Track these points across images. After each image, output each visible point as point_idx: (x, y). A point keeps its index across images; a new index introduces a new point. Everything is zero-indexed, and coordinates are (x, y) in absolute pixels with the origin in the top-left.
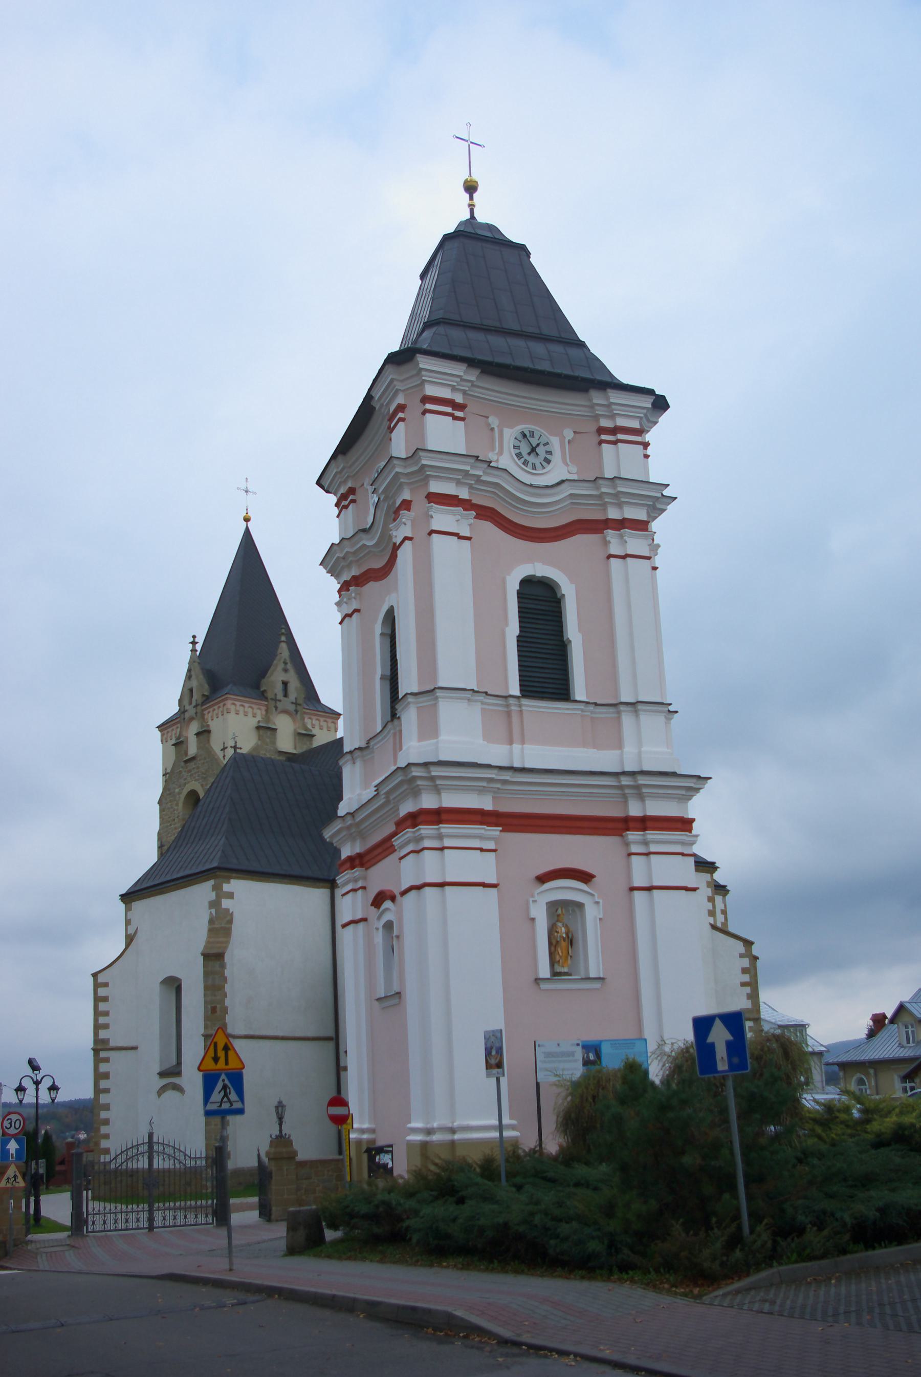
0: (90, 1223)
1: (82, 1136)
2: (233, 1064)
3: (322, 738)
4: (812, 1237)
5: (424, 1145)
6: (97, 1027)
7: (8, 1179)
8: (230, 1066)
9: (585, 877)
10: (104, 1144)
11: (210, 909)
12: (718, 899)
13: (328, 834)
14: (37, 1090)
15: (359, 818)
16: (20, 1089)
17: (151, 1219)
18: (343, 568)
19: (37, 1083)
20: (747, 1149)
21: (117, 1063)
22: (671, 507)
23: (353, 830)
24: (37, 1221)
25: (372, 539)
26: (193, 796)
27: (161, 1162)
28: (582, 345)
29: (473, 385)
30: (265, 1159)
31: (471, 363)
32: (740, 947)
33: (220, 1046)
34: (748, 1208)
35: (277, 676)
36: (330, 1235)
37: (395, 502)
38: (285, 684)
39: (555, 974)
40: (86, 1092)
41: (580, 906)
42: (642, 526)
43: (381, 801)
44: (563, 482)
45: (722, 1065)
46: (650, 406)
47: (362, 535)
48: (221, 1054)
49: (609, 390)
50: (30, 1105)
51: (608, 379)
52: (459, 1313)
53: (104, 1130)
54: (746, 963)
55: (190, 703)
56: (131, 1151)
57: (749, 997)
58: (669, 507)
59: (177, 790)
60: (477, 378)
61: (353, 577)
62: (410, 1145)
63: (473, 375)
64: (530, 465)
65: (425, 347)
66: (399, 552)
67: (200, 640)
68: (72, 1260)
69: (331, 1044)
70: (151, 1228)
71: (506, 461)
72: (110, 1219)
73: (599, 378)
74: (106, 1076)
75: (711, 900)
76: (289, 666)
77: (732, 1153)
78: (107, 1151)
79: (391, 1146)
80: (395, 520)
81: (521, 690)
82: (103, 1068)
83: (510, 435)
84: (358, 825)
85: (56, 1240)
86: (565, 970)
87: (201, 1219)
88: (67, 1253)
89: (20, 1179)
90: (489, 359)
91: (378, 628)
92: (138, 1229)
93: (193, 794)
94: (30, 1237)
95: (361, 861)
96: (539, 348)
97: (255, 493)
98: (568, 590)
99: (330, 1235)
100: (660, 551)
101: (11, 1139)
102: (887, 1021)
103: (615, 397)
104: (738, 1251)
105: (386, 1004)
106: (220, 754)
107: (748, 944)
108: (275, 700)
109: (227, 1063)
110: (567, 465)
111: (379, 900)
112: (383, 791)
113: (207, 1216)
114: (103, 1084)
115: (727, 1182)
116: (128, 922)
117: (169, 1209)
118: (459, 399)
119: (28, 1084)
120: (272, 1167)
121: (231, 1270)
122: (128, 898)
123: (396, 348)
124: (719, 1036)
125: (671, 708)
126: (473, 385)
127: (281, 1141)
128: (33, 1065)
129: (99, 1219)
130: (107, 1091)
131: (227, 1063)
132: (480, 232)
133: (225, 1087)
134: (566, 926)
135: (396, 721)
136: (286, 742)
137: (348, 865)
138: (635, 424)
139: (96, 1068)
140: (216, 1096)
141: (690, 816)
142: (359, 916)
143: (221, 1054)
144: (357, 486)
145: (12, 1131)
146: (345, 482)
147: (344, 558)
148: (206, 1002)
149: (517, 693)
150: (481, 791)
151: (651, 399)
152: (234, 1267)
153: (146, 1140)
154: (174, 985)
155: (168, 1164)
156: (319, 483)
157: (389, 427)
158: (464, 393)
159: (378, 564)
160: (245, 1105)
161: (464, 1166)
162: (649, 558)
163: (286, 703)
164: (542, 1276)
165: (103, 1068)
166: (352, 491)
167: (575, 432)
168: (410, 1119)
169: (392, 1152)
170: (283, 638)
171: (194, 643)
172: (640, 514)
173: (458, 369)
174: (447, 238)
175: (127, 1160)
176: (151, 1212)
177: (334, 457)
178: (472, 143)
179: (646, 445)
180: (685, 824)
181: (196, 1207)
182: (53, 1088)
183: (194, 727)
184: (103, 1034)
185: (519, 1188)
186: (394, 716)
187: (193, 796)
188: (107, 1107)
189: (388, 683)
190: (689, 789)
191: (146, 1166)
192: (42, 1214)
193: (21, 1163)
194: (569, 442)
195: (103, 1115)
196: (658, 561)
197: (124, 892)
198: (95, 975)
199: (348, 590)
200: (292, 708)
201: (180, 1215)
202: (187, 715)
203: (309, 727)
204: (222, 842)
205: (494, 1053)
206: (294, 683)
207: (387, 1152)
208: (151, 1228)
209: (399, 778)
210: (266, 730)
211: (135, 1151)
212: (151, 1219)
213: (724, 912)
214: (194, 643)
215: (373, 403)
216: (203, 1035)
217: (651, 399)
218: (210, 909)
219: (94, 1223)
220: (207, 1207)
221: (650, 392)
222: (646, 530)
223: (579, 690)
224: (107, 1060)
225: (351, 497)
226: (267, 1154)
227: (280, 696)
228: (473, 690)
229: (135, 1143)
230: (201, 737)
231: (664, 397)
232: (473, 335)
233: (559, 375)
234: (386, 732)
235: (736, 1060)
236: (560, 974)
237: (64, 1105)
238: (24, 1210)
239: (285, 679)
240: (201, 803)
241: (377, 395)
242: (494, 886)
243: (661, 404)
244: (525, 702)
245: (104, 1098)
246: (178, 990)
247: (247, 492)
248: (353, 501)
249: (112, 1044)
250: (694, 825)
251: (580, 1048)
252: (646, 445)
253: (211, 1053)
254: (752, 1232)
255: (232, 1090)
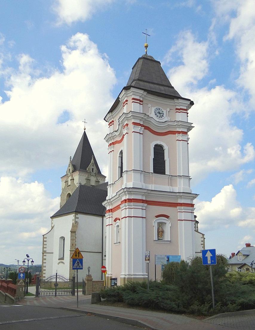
0: (40, 294)
1: (38, 273)
2: (80, 257)
3: (101, 182)
4: (230, 306)
5: (125, 278)
6: (43, 248)
7: (20, 283)
8: (80, 257)
9: (167, 217)
10: (44, 275)
11: (73, 221)
12: (196, 224)
13: (103, 204)
14: (28, 262)
15: (111, 200)
16: (24, 261)
17: (56, 294)
18: (110, 140)
19: (28, 260)
20: (215, 284)
21: (48, 256)
22: (193, 129)
23: (110, 203)
24: (27, 293)
25: (117, 133)
26: (69, 195)
27: (59, 280)
28: (173, 88)
29: (145, 96)
30: (84, 280)
31: (145, 90)
32: (201, 236)
33: (77, 253)
34: (214, 298)
35: (91, 166)
36: (102, 299)
37: (124, 124)
38: (93, 169)
39: (159, 239)
40: (40, 263)
41: (165, 223)
42: (186, 133)
43: (117, 196)
44: (166, 121)
45: (209, 262)
46: (189, 103)
47: (115, 132)
48: (77, 254)
49: (179, 99)
50: (26, 266)
51: (179, 96)
52: (139, 321)
53: (44, 272)
54: (203, 239)
55: (69, 172)
56: (51, 277)
57: (203, 247)
58: (193, 129)
59: (65, 193)
60: (146, 94)
61: (112, 142)
62: (121, 278)
63: (145, 93)
64: (158, 117)
65: (133, 86)
66: (125, 137)
67: (72, 157)
68: (35, 302)
69: (101, 254)
70: (56, 296)
71: (152, 115)
72: (46, 293)
73: (178, 96)
74: (45, 259)
75: (195, 224)
76: (94, 165)
77: (211, 284)
78: (45, 277)
79: (117, 278)
80: (124, 129)
81: (154, 172)
82: (44, 257)
83: (153, 109)
84: (111, 202)
85: (32, 298)
86: (161, 238)
87: (68, 294)
88: (34, 301)
89: (23, 283)
90: (150, 90)
91: (118, 155)
92: (52, 296)
93: (69, 194)
94: (25, 297)
95: (111, 210)
96: (162, 88)
97: (87, 123)
98: (166, 148)
99: (102, 299)
100: (189, 139)
101: (21, 274)
102: (235, 255)
103: (180, 101)
104: (212, 309)
105: (116, 245)
106: (76, 185)
107: (203, 235)
108: (90, 173)
109: (79, 257)
110: (167, 117)
111: (115, 220)
112: (118, 194)
113: (70, 293)
114: (44, 261)
115: (209, 292)
116: (52, 223)
117: (60, 291)
118: (141, 99)
119: (26, 260)
120: (86, 282)
121: (78, 307)
122: (52, 217)
123: (126, 86)
124: (209, 255)
125: (190, 178)
126: (145, 96)
127: (89, 276)
128: (28, 256)
129: (43, 293)
130: (45, 263)
131: (79, 257)
132: (148, 58)
133: (78, 262)
134: (162, 228)
135: (122, 178)
136: (93, 183)
137: (108, 211)
138: (185, 108)
139: (43, 257)
140: (76, 265)
141: (194, 204)
142: (110, 224)
143: (77, 254)
144: (114, 120)
145: (22, 271)
146: (111, 119)
147: (110, 138)
148: (71, 243)
149: (153, 172)
150: (143, 195)
151: (190, 102)
152: (79, 307)
153: (55, 275)
154: (63, 238)
155: (61, 281)
156: (104, 119)
157: (123, 106)
158: (143, 98)
159: (119, 139)
160: (83, 267)
161: (138, 284)
162: (187, 141)
163: (93, 174)
164: (161, 312)
165: (44, 257)
166: (113, 121)
167: (170, 109)
168: (121, 272)
169: (117, 280)
170: (93, 158)
171: (71, 158)
172: (185, 130)
173: (142, 92)
174: (140, 59)
175: (50, 279)
176: (56, 292)
177: (109, 113)
178: (147, 35)
179: (188, 113)
180: (192, 205)
181: (67, 291)
182: (32, 261)
183: (70, 178)
184: (45, 249)
185: (153, 290)
186: (121, 176)
187: (69, 195)
188: (45, 267)
189: (120, 169)
190: (193, 197)
191: (55, 281)
192: (28, 291)
193: (23, 279)
194: (168, 111)
195: (44, 268)
196: (189, 142)
197: (51, 216)
198: (43, 235)
199: (111, 145)
200: (94, 175)
201: (66, 293)
202: (68, 175)
203: (98, 179)
204: (76, 205)
205: (147, 257)
206: (95, 169)
207: (116, 280)
208: (56, 296)
209: (122, 191)
210: (88, 180)
211: (52, 277)
212: (56, 294)
213: (197, 227)
214: (71, 158)
215: (119, 99)
216: (70, 251)
217: (190, 102)
218: (73, 221)
219: (41, 294)
220: (70, 291)
221: (190, 100)
222: (187, 134)
223: (167, 172)
224: (46, 256)
225: (112, 123)
226: (85, 279)
227: (92, 172)
228: (142, 171)
229: (50, 276)
230: (71, 181)
231: (193, 102)
232: (145, 83)
233: (167, 95)
234: (119, 180)
235: (213, 261)
236: (160, 239)
237: (35, 266)
238: (24, 290)
239: (93, 168)
240: (71, 196)
241: (120, 97)
242: (145, 218)
243: (192, 103)
244: (154, 174)
245: (44, 265)
246: (64, 239)
247: (85, 122)
248: (127, 104)
249: (47, 252)
250: (194, 206)
251: (166, 257)
252: (188, 113)
253: (75, 254)
254: (215, 304)
255: (80, 263)
